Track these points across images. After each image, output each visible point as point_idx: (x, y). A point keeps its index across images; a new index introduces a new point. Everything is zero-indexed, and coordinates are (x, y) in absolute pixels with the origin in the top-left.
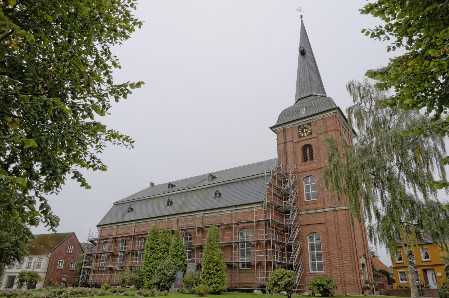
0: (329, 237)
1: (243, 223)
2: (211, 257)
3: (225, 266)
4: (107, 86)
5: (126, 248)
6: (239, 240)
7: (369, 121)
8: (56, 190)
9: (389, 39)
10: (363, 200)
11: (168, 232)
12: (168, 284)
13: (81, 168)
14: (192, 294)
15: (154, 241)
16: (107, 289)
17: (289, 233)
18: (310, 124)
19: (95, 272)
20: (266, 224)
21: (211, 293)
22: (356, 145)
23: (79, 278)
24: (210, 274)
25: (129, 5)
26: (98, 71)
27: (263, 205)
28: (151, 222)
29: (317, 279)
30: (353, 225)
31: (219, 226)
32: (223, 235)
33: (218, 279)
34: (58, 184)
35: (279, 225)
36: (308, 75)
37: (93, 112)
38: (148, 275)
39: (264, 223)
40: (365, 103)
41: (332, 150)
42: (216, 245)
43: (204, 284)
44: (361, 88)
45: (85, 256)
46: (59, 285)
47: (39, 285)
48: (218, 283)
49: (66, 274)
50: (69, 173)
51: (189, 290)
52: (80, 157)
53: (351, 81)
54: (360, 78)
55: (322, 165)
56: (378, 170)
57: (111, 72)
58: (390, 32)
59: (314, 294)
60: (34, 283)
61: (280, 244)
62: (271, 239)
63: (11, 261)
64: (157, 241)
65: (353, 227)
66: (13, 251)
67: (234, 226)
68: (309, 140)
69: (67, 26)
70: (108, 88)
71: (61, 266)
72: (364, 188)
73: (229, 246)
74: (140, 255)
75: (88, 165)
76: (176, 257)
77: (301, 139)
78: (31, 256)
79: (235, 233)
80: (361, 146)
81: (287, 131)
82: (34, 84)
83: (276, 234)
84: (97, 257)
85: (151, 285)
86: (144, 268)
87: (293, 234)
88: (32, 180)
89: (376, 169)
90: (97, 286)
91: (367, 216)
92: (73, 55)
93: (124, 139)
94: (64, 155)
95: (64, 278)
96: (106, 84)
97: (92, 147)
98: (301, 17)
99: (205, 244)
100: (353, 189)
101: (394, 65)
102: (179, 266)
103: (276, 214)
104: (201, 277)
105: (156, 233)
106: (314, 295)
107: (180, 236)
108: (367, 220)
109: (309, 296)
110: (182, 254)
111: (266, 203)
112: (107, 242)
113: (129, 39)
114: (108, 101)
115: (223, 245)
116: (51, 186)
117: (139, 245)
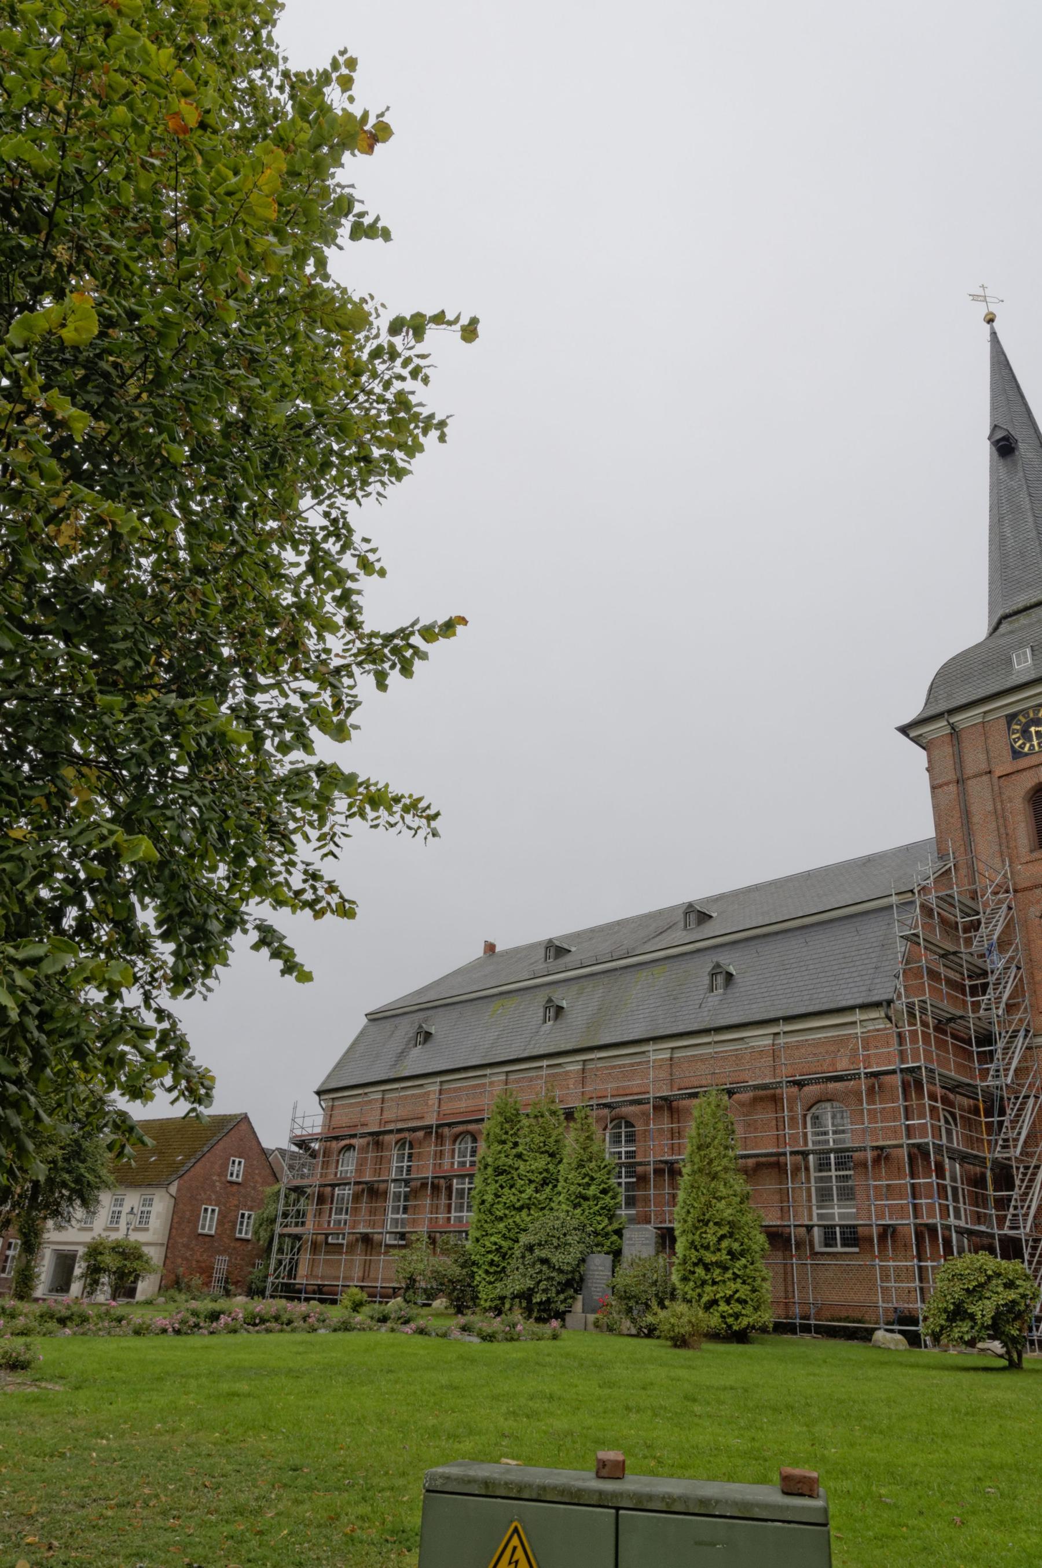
1: (817, 1081)
3: (762, 1238)
4: (343, 636)
5: (413, 1169)
6: (806, 1144)
8: (203, 984)
11: (553, 1113)
12: (562, 1297)
13: (275, 908)
14: (649, 1336)
16: (357, 1307)
17: (996, 1119)
19: (315, 1247)
20: (905, 1086)
21: (714, 1336)
23: (267, 1267)
24: (707, 1268)
25: (405, 372)
26: (315, 593)
27: (891, 1013)
28: (494, 1079)
31: (730, 1093)
32: (748, 1125)
33: (738, 1285)
34: (208, 968)
35: (955, 1088)
36: (1030, 524)
37: (313, 732)
38: (492, 1263)
39: (897, 1079)
42: (725, 1162)
43: (690, 1301)
45: (282, 1196)
46: (205, 1290)
47: (145, 1288)
48: (739, 1301)
49: (225, 1251)
50: (245, 931)
51: (634, 1321)
52: (274, 875)
57: (359, 592)
60: (132, 1278)
61: (964, 1158)
62: (929, 1139)
63: (64, 1204)
64: (516, 1144)
66: (69, 1172)
67: (786, 1092)
69: (222, 468)
71: (208, 1225)
73: (772, 1166)
74: (461, 1193)
75: (296, 901)
77: (1023, 763)
78: (120, 1191)
82: (137, 658)
83: (947, 1122)
84: (321, 1199)
85: (502, 1299)
87: (1014, 1122)
88: (130, 954)
90: (326, 1295)
92: (243, 552)
93: (406, 809)
94: (222, 870)
95: (221, 1264)
96: (343, 631)
98: (990, 321)
99: (685, 1157)
102: (596, 1233)
103: (941, 1044)
104: (675, 1278)
105: (511, 1119)
107: (594, 1128)
110: (604, 1192)
111: (901, 1005)
112: (350, 1147)
113: (405, 479)
114: (351, 687)
115: (751, 1162)
116: (191, 974)
117: (455, 1158)
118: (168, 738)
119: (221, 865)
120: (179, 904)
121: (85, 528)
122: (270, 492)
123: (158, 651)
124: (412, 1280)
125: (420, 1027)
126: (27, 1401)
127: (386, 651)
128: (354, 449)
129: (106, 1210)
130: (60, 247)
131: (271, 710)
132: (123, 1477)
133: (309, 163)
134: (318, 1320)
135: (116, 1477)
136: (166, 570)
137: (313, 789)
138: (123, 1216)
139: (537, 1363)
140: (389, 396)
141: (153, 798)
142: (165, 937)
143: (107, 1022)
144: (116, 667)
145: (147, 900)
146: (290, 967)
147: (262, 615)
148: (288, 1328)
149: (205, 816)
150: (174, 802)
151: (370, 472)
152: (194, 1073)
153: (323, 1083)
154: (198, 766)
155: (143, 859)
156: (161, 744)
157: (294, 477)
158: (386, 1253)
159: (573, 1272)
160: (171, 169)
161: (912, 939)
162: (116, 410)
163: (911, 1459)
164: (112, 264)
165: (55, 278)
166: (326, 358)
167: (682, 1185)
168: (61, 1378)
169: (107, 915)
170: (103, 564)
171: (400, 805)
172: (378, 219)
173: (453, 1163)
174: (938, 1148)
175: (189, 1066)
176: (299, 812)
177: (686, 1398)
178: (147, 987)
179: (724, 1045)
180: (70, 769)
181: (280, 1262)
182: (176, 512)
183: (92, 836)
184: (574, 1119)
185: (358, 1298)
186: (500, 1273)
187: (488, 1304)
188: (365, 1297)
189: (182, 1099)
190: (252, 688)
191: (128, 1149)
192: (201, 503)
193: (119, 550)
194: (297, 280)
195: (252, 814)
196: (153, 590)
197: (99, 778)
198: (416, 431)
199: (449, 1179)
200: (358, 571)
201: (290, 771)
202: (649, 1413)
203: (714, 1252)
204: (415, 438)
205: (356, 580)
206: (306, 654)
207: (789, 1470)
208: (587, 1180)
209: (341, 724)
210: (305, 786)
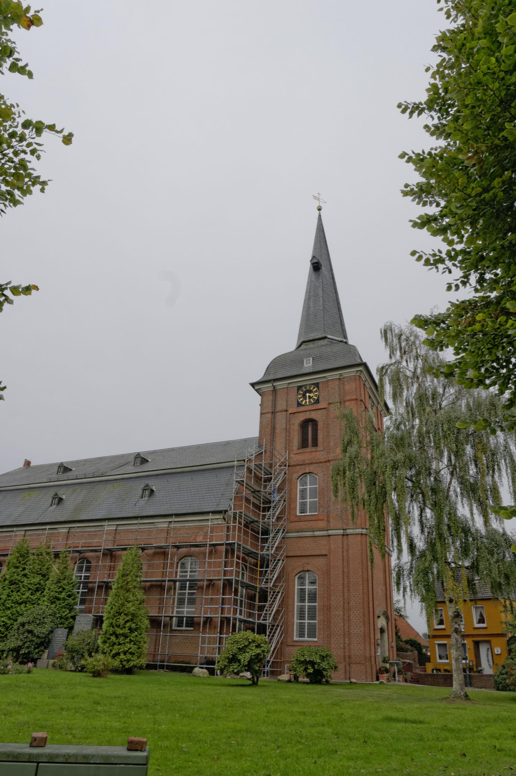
7: (410, 393)
9: (450, 272)
10: (390, 522)
11: (48, 554)
12: (37, 651)
14: (80, 671)
15: (19, 570)
18: (317, 385)
22: (388, 428)
24: (117, 636)
25: (28, 150)
27: (226, 516)
30: (372, 562)
31: (143, 549)
33: (131, 645)
35: (249, 554)
36: (321, 304)
39: (223, 548)
40: (407, 361)
41: (348, 434)
43: (104, 653)
44: (403, 337)
48: (132, 654)
51: (74, 663)
53: (389, 324)
55: (331, 456)
56: (418, 473)
58: (453, 262)
59: (298, 677)
64: (24, 569)
65: (372, 566)
67: (170, 551)
68: (313, 413)
72: (395, 502)
76: (58, 602)
77: (301, 409)
79: (172, 564)
81: (278, 392)
91: (395, 548)
98: (319, 210)
100: (377, 501)
101: (455, 312)
102: (61, 618)
106: (297, 681)
107: (69, 563)
108: (394, 555)
109: (289, 681)
110: (69, 596)
115: (148, 584)
139: (17, 686)
140: (16, 160)
159: (45, 638)
177: (95, 703)
179: (144, 526)
208: (61, 589)
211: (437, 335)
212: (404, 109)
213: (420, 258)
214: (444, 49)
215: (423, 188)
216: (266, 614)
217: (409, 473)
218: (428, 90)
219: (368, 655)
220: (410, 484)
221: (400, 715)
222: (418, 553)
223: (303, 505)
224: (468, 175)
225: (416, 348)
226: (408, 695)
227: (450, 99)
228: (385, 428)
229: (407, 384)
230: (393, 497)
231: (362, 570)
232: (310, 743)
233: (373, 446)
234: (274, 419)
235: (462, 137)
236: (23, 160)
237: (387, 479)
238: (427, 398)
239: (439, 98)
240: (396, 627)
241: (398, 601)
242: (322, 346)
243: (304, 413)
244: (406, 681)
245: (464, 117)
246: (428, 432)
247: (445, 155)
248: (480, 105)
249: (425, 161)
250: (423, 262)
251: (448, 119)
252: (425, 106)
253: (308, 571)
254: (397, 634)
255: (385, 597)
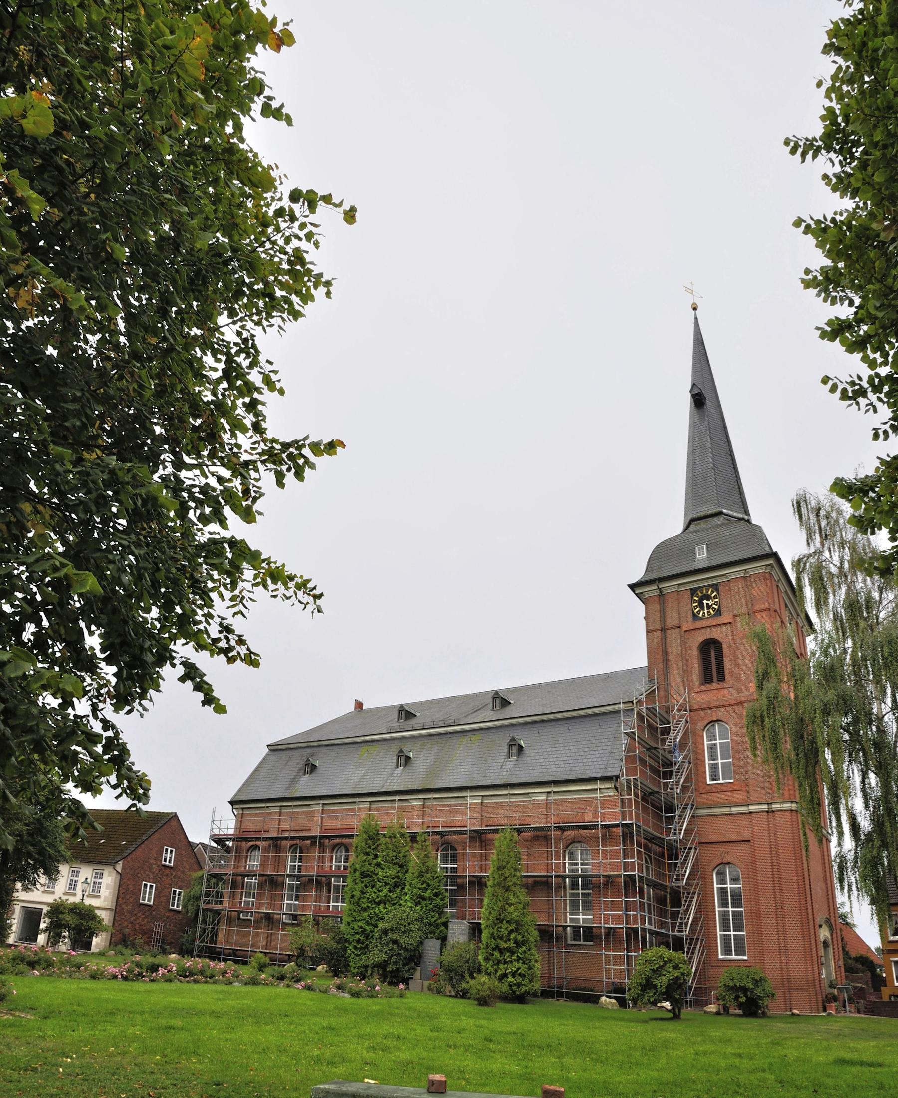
0: (759, 875)
2: (503, 909)
4: (251, 437)
6: (565, 871)
7: (837, 598)
8: (140, 704)
9: (875, 411)
10: (826, 792)
11: (402, 835)
12: (406, 968)
13: (197, 650)
14: (463, 997)
15: (370, 857)
16: (262, 968)
18: (715, 587)
19: (230, 922)
22: (813, 653)
24: (501, 952)
25: (302, 234)
26: (229, 396)
27: (618, 785)
29: (734, 975)
30: (807, 850)
31: (519, 831)
33: (520, 965)
35: (651, 839)
36: (710, 458)
37: (227, 511)
38: (358, 941)
39: (620, 830)
40: (830, 550)
41: (763, 662)
42: (514, 879)
43: (489, 974)
44: (822, 513)
45: (205, 880)
46: (146, 948)
47: (98, 942)
48: (521, 975)
50: (173, 666)
51: (453, 986)
53: (801, 492)
54: (820, 491)
55: (744, 696)
56: (856, 721)
57: (264, 404)
58: (878, 394)
59: (728, 1009)
64: (376, 856)
65: (807, 856)
66: (33, 845)
67: (554, 833)
70: (254, 443)
71: (148, 897)
72: (829, 763)
75: (213, 647)
76: (423, 903)
77: (699, 624)
79: (557, 852)
80: (823, 659)
81: (667, 598)
82: (84, 419)
84: (234, 885)
85: (366, 967)
86: (349, 924)
87: (683, 864)
89: (853, 716)
90: (240, 958)
91: (835, 830)
93: (298, 587)
94: (155, 612)
96: (251, 433)
97: (223, 599)
98: (695, 309)
100: (807, 762)
101: (886, 474)
102: (430, 924)
103: (645, 809)
106: (728, 1012)
107: (430, 849)
108: (834, 840)
109: (718, 1013)
110: (436, 895)
112: (256, 847)
114: (257, 480)
115: (531, 880)
116: (130, 695)
117: (334, 863)
118: (110, 493)
119: (154, 608)
120: (120, 635)
121: (40, 297)
122: (195, 304)
123: (102, 417)
124: (302, 951)
125: (308, 760)
126: (5, 1026)
127: (284, 456)
128: (261, 286)
129: (66, 877)
130: (22, 47)
131: (194, 486)
132: (85, 1087)
133: (230, 44)
134: (233, 976)
135: (79, 1088)
136: (109, 350)
137: (227, 558)
138: (79, 885)
139: (390, 1014)
140: (289, 249)
141: (98, 541)
142: (109, 661)
143: (61, 724)
144: (66, 424)
145: (93, 627)
146: (209, 700)
147: (187, 406)
148: (211, 981)
149: (140, 565)
150: (115, 548)
151: (274, 308)
152: (133, 775)
153: (235, 796)
154: (135, 522)
155: (89, 592)
156: (105, 497)
157: (213, 296)
158: (283, 930)
159: (414, 950)
160: (118, 11)
161: (630, 735)
162: (69, 202)
163: (618, 1079)
164: (66, 75)
165: (17, 73)
166: (241, 205)
167: (487, 895)
168: (32, 1009)
169: (60, 635)
170: (57, 332)
171: (294, 583)
172: (282, 106)
173: (331, 866)
174: (641, 878)
175: (130, 769)
176: (215, 575)
177: (486, 1039)
178: (94, 701)
180: (28, 504)
181: (204, 930)
182: (118, 302)
183: (47, 565)
184: (416, 841)
185: (263, 961)
186: (365, 949)
187: (356, 970)
188: (267, 960)
189: (124, 795)
190: (179, 465)
191: (82, 831)
192: (138, 299)
193: (69, 323)
194: (219, 135)
195: (178, 569)
196: (98, 364)
197: (52, 517)
198: (309, 284)
199: (329, 878)
200: (262, 385)
201: (209, 539)
202: (462, 1049)
203: (506, 942)
204: (308, 289)
205: (262, 393)
206: (222, 445)
207: (547, 1086)
208: (424, 886)
209: (249, 508)
210: (221, 554)
211: (865, 509)
212: (793, 147)
213: (833, 389)
214: (838, 51)
215: (830, 276)
216: (681, 923)
217: (845, 720)
218: (823, 118)
219: (810, 978)
220: (846, 737)
221: (855, 1056)
222: (862, 837)
223: (714, 768)
224: (886, 255)
225: (841, 530)
226: (863, 1030)
227: (853, 133)
228: (809, 653)
229: (832, 586)
230: (826, 756)
231: (796, 862)
232: (750, 1093)
233: (796, 680)
234: (664, 639)
235: (873, 195)
236: (297, 250)
237: (818, 730)
238: (860, 607)
239: (838, 131)
240: (842, 939)
241: (842, 904)
242: (718, 526)
243: (703, 630)
244: (859, 1012)
245: (874, 161)
246: (864, 659)
247: (854, 223)
248: (894, 142)
249: (829, 231)
250: (838, 393)
251: (853, 164)
252: (820, 143)
253: (729, 863)
254: (843, 949)
255: (825, 899)
